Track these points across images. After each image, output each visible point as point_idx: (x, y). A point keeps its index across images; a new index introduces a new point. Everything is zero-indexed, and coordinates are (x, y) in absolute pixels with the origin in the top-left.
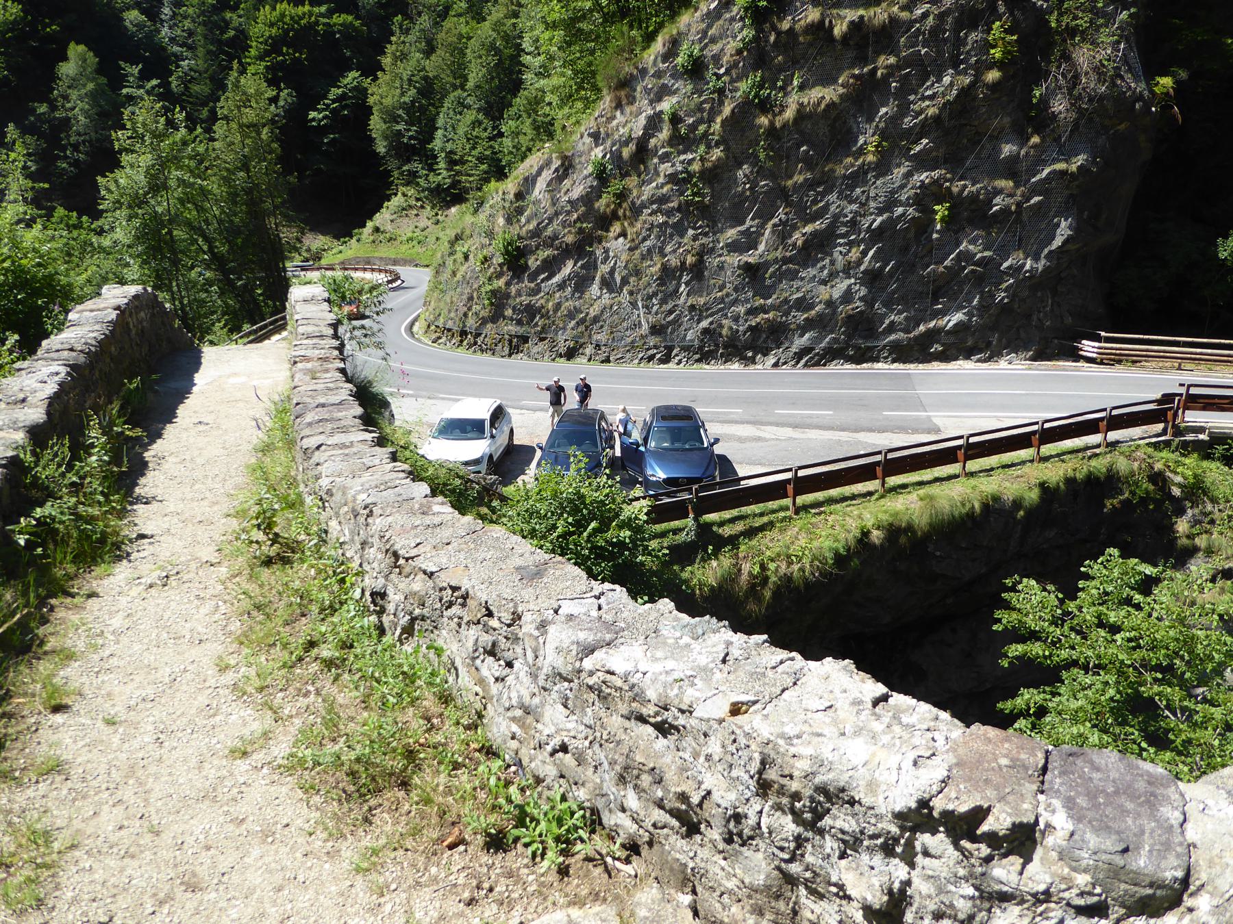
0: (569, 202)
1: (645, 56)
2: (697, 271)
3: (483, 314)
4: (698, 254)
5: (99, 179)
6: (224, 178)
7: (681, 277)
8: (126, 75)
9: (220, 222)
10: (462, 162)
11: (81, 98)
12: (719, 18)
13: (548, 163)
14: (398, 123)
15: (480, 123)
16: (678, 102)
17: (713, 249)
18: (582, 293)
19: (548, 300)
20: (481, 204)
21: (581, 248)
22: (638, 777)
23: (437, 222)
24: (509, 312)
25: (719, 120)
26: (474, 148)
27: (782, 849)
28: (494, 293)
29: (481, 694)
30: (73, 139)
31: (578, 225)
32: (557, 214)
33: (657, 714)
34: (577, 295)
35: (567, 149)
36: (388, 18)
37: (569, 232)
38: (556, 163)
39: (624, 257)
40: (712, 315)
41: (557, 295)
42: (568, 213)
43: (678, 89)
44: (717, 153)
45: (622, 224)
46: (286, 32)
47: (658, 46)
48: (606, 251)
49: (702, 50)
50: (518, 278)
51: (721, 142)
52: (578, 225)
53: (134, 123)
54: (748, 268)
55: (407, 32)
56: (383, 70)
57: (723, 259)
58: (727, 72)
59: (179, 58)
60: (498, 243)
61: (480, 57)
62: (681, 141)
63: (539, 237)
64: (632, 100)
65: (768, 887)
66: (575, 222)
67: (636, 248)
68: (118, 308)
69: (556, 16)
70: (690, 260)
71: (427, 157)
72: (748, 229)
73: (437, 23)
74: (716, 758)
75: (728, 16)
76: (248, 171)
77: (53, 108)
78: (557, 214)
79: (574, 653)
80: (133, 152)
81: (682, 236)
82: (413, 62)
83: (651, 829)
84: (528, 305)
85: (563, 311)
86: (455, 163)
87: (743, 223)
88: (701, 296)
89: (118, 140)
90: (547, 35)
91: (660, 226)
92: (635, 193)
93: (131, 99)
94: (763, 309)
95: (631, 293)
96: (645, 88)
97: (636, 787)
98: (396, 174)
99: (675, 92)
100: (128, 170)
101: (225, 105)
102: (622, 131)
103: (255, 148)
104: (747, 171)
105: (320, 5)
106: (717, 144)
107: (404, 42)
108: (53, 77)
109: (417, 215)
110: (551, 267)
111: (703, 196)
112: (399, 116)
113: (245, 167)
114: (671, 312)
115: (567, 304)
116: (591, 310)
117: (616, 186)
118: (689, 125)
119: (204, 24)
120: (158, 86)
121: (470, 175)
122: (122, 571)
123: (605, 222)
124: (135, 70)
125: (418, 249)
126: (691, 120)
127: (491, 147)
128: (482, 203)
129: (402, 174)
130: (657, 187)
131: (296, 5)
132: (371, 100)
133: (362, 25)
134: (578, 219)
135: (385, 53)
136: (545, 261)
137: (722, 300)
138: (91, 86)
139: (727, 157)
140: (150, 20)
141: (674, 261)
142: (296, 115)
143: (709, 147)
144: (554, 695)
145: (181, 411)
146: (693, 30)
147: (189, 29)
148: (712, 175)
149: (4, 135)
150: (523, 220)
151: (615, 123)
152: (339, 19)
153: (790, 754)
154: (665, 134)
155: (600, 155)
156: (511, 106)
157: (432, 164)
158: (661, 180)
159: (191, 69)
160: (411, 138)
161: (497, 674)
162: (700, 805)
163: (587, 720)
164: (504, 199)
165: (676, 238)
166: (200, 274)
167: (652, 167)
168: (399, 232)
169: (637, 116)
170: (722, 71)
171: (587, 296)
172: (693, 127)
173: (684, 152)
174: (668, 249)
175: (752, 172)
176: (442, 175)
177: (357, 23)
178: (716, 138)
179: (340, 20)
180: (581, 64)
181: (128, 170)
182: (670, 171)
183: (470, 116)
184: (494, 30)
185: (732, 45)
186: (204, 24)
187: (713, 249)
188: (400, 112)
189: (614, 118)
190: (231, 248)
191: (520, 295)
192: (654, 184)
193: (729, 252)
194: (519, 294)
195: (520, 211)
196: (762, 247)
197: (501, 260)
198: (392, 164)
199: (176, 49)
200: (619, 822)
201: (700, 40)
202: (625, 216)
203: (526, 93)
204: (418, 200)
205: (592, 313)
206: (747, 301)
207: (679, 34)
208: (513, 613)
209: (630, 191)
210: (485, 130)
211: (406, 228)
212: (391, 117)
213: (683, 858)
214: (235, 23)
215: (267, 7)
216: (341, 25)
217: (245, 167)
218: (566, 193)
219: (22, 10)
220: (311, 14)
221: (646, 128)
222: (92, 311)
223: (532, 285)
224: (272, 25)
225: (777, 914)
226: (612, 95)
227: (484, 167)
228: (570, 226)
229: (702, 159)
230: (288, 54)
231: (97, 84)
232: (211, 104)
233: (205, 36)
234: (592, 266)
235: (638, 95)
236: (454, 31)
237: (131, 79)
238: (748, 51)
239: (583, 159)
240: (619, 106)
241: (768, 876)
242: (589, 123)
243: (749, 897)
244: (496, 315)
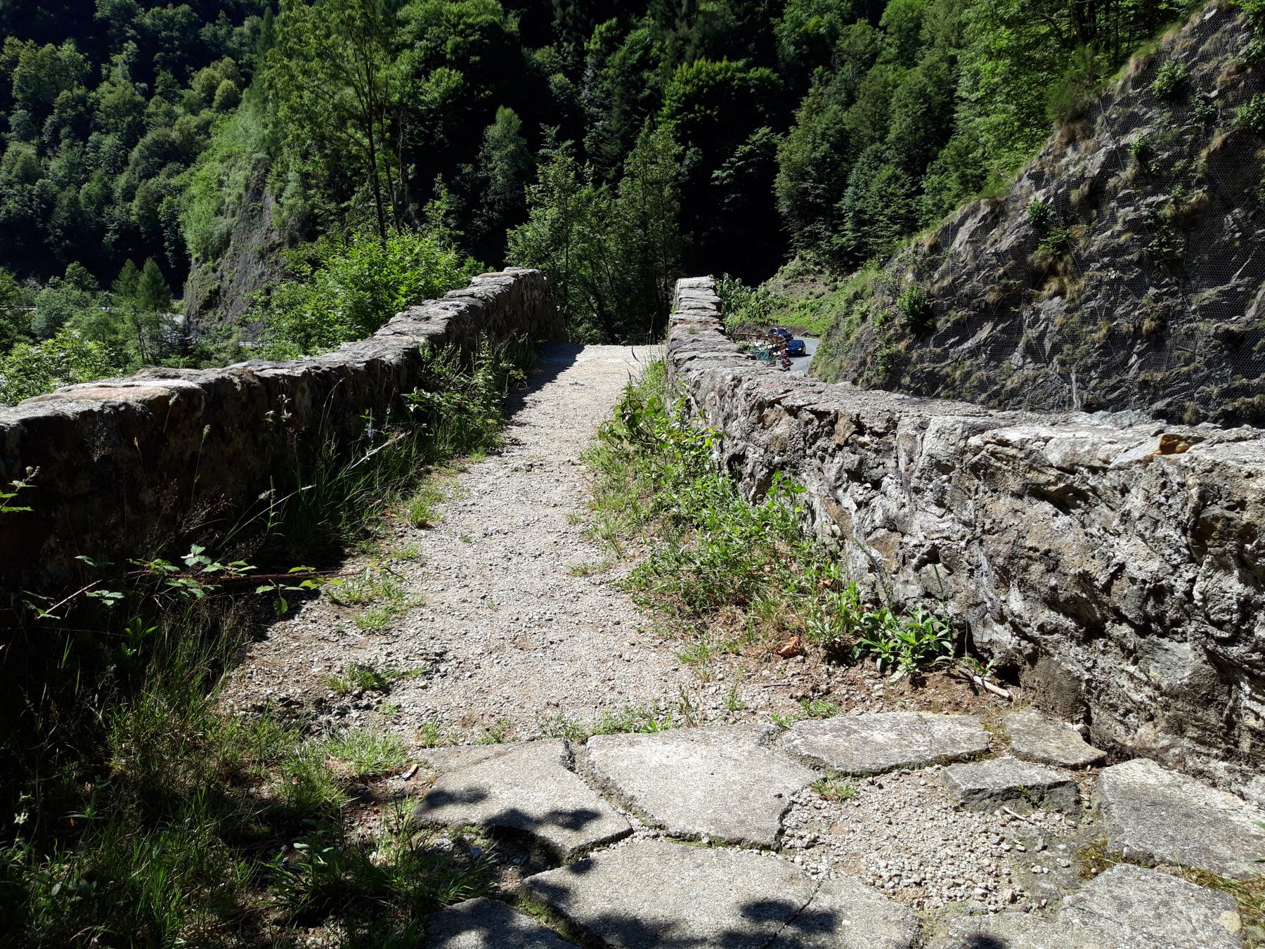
0: (995, 254)
1: (1111, 81)
2: (1157, 340)
4: (1159, 318)
5: (509, 231)
6: (621, 235)
7: (1132, 346)
8: (544, 137)
9: (613, 279)
10: (872, 222)
11: (501, 159)
12: (1216, 30)
13: (975, 210)
14: (805, 180)
15: (897, 178)
16: (1150, 134)
17: (1181, 313)
18: (1000, 361)
19: (955, 369)
20: (888, 258)
21: (1004, 310)
22: (1025, 569)
23: (835, 289)
24: (906, 380)
25: (1204, 153)
26: (887, 206)
27: (1219, 625)
28: (891, 358)
29: (839, 533)
30: (490, 197)
31: (1003, 281)
32: (978, 269)
33: (1059, 479)
34: (992, 363)
35: (1000, 194)
36: (809, 69)
37: (992, 289)
38: (985, 210)
39: (1059, 320)
40: (1169, 395)
41: (968, 363)
42: (993, 267)
43: (1151, 118)
44: (1198, 195)
45: (1061, 281)
46: (700, 89)
47: (1130, 68)
48: (1037, 312)
49: (1188, 70)
50: (923, 341)
51: (1208, 179)
52: (1003, 281)
53: (546, 178)
54: (1229, 338)
55: (827, 83)
56: (797, 125)
57: (1194, 325)
58: (1221, 95)
59: (595, 118)
60: (904, 301)
61: (906, 106)
62: (1149, 180)
63: (953, 294)
64: (1089, 133)
65: (1194, 687)
66: (1000, 278)
67: (1076, 309)
69: (1004, 43)
70: (1147, 324)
71: (833, 216)
72: (1234, 289)
73: (862, 72)
74: (1136, 514)
75: (1229, 26)
76: (645, 229)
77: (477, 168)
78: (978, 269)
79: (959, 431)
80: (542, 205)
81: (1140, 296)
82: (829, 115)
83: (1037, 634)
84: (930, 373)
86: (864, 223)
87: (1228, 281)
88: (1158, 370)
89: (530, 193)
90: (990, 65)
91: (1111, 283)
92: (1082, 243)
93: (546, 159)
94: (1247, 391)
95: (1063, 363)
96: (1108, 119)
97: (1022, 583)
98: (796, 236)
99: (1147, 122)
100: (535, 224)
101: (632, 162)
102: (1072, 170)
103: (655, 206)
104: (1238, 216)
105: (738, 59)
106: (1200, 183)
107: (822, 94)
108: (480, 139)
109: (813, 281)
110: (963, 329)
111: (1175, 247)
112: (807, 173)
113: (644, 225)
114: (1114, 388)
115: (979, 373)
116: (1009, 382)
117: (1057, 235)
118: (1163, 161)
119: (623, 84)
120: (572, 146)
121: (878, 237)
122: (491, 462)
123: (1038, 278)
124: (553, 131)
125: (809, 316)
126: (1166, 155)
127: (907, 205)
128: (890, 257)
129: (803, 236)
130: (1112, 236)
131: (714, 61)
133: (779, 78)
134: (1005, 274)
136: (957, 323)
137: (1188, 376)
138: (512, 147)
139: (1212, 198)
140: (572, 82)
141: (1126, 326)
142: (700, 173)
143: (1187, 187)
144: (929, 496)
145: (560, 376)
146: (1178, 48)
147: (608, 90)
148: (1187, 222)
150: (936, 276)
151: (1064, 161)
153: (1244, 473)
154: (1129, 172)
155: (1041, 199)
156: (936, 158)
157: (838, 225)
159: (604, 130)
160: (817, 196)
161: (860, 498)
162: (1107, 588)
163: (966, 515)
164: (916, 252)
165: (1131, 299)
166: (587, 330)
167: (1107, 212)
168: (791, 298)
169: (1093, 152)
170: (1214, 94)
171: (1005, 364)
172: (1169, 163)
173: (1153, 194)
174: (1119, 311)
175: (1245, 217)
176: (847, 237)
177: (774, 77)
178: (1199, 175)
179: (758, 74)
180: (1026, 100)
181: (535, 224)
182: (1131, 216)
183: (886, 171)
184: (925, 75)
185: (1230, 63)
186: (623, 84)
187: (1181, 313)
188: (809, 169)
189: (1064, 155)
190: (619, 307)
191: (922, 362)
192: (1108, 233)
193: (1204, 317)
194: (921, 359)
195: (934, 266)
196: (1251, 313)
197: (904, 321)
198: (794, 224)
199: (593, 110)
200: (995, 637)
201: (1187, 59)
202: (1065, 271)
203: (956, 143)
204: (816, 264)
205: (1009, 385)
206: (1223, 379)
207: (1159, 53)
208: (888, 421)
209: (1076, 241)
210: (903, 186)
211: (800, 295)
212: (799, 174)
213: (1077, 669)
214: (651, 83)
215: (685, 64)
216: (757, 79)
217: (644, 225)
218: (993, 244)
219: (463, 78)
220: (727, 69)
221: (1104, 166)
223: (938, 350)
224: (687, 82)
225: (1204, 729)
226: (1064, 129)
227: (896, 227)
228: (993, 282)
229: (1177, 202)
230: (700, 111)
231: (518, 145)
232: (619, 164)
233: (622, 97)
235: (1097, 128)
236: (879, 79)
237: (549, 140)
238: (1254, 67)
239: (1019, 204)
240: (1072, 141)
241: (1195, 672)
242: (1031, 163)
243: (1166, 707)
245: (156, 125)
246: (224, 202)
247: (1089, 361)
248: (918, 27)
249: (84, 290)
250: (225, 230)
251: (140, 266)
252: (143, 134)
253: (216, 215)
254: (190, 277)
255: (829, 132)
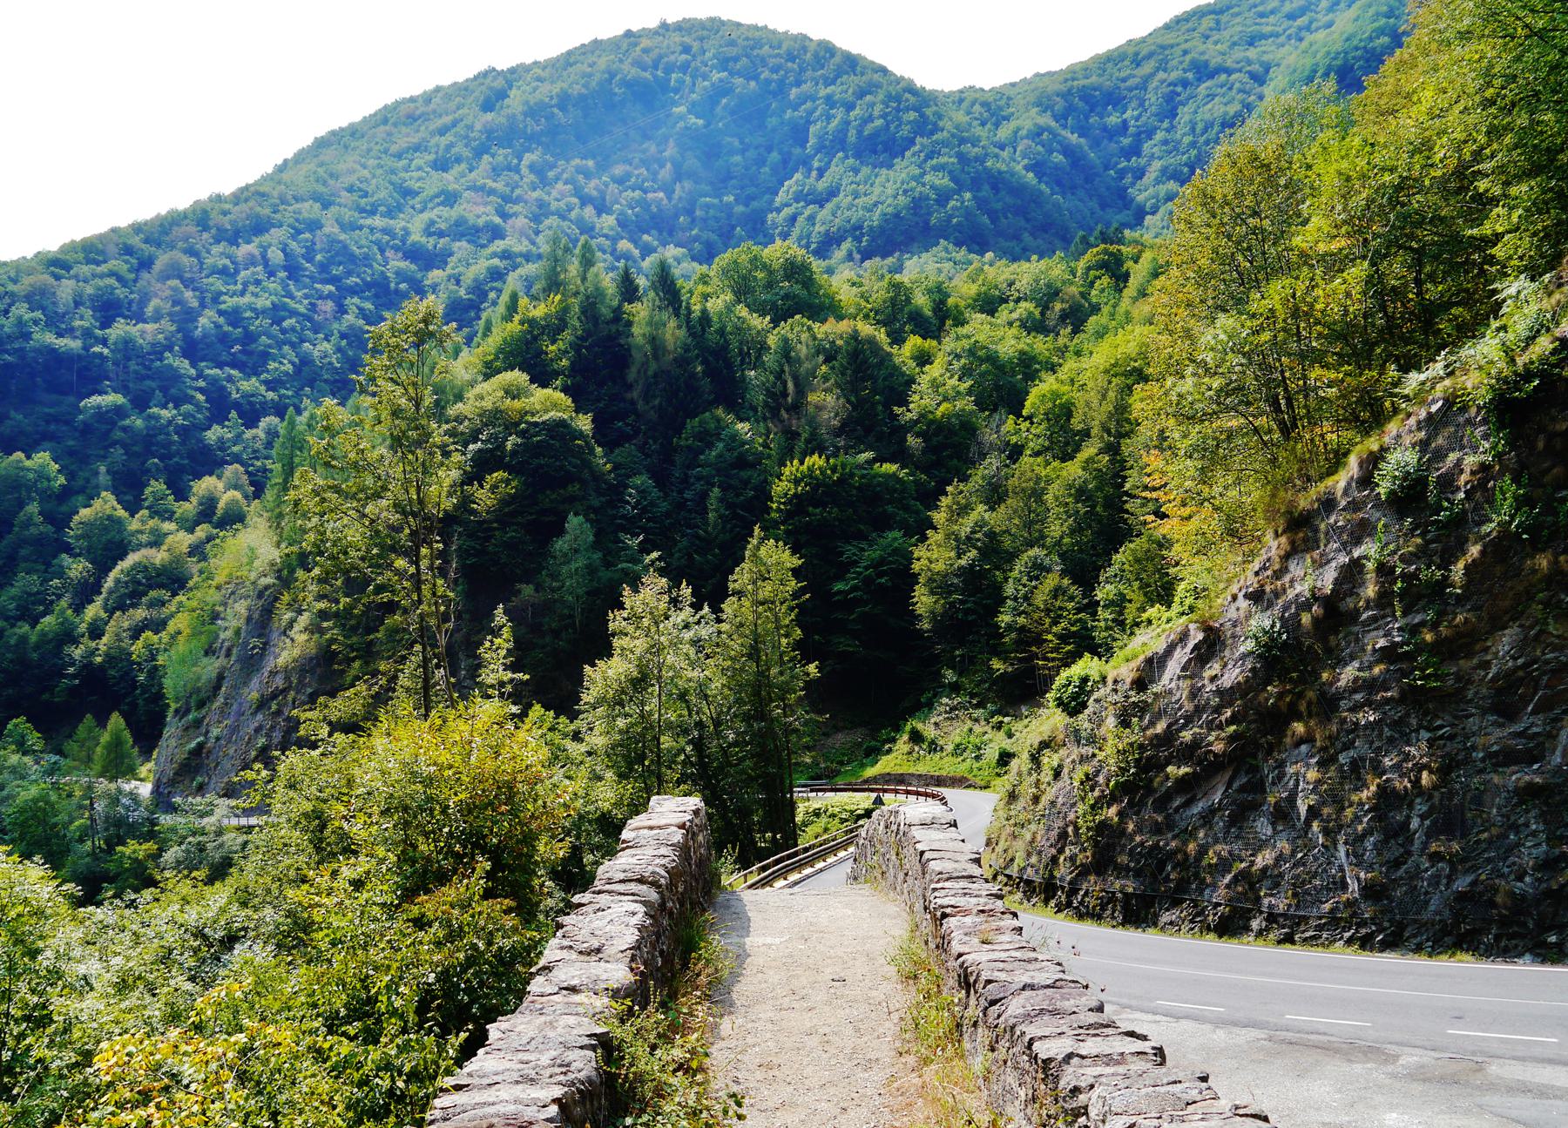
3: (1080, 858)
5: (587, 668)
13: (1184, 637)
26: (1055, 623)
28: (1102, 827)
32: (1199, 710)
38: (1197, 636)
56: (935, 528)
68: (682, 826)
78: (1199, 710)
85: (1211, 858)
101: (741, 578)
120: (659, 559)
132: (916, 567)
135: (937, 507)
149: (491, 617)
152: (889, 468)
158: (1368, 658)
182: (1382, 643)
211: (956, 733)
222: (651, 828)
234: (1258, 787)
244: (1102, 864)
245: (140, 546)
246: (217, 636)
247: (1360, 828)
248: (1069, 415)
249: (24, 754)
250: (214, 675)
251: (102, 722)
252: (122, 556)
253: (206, 654)
254: (166, 734)
255: (978, 536)
